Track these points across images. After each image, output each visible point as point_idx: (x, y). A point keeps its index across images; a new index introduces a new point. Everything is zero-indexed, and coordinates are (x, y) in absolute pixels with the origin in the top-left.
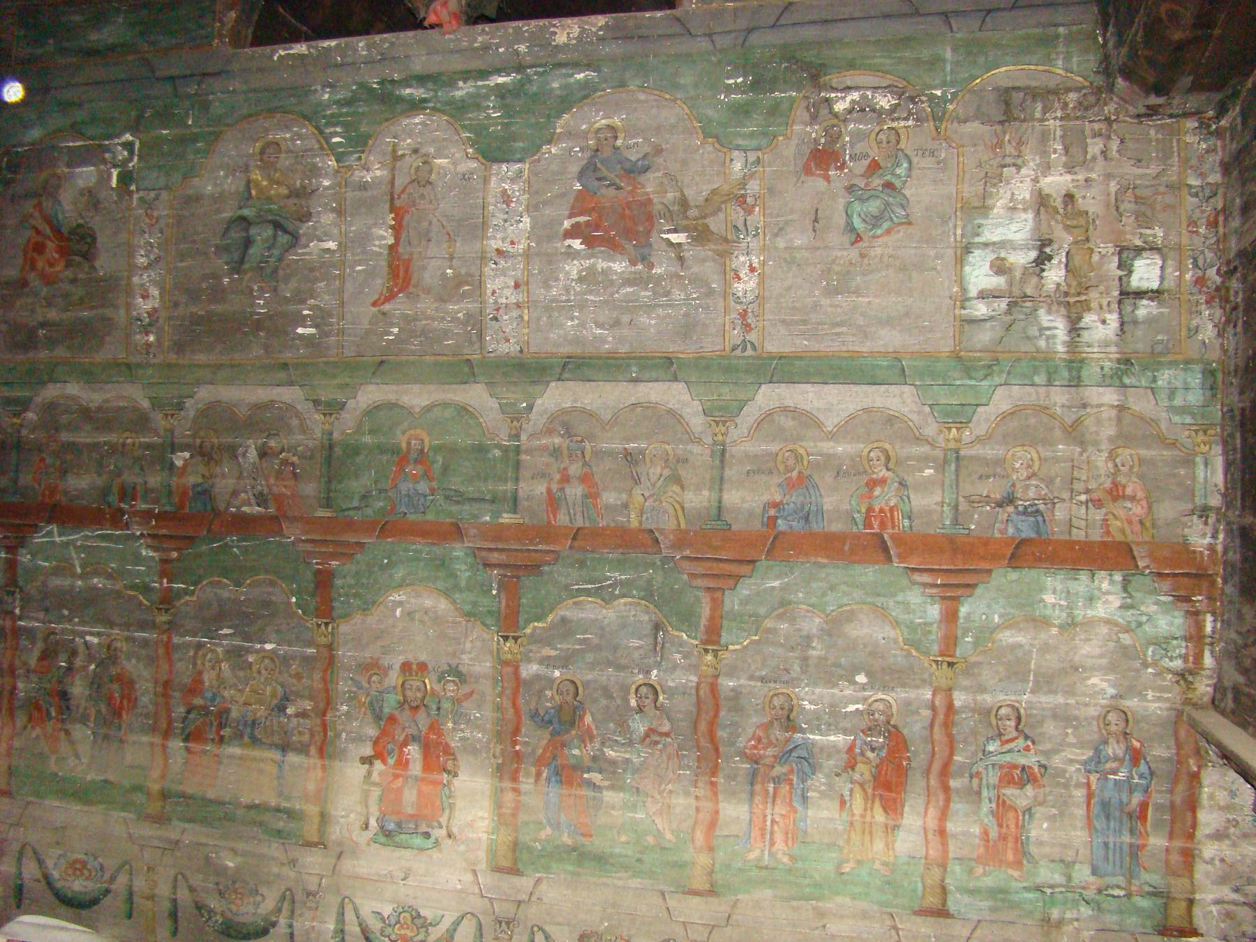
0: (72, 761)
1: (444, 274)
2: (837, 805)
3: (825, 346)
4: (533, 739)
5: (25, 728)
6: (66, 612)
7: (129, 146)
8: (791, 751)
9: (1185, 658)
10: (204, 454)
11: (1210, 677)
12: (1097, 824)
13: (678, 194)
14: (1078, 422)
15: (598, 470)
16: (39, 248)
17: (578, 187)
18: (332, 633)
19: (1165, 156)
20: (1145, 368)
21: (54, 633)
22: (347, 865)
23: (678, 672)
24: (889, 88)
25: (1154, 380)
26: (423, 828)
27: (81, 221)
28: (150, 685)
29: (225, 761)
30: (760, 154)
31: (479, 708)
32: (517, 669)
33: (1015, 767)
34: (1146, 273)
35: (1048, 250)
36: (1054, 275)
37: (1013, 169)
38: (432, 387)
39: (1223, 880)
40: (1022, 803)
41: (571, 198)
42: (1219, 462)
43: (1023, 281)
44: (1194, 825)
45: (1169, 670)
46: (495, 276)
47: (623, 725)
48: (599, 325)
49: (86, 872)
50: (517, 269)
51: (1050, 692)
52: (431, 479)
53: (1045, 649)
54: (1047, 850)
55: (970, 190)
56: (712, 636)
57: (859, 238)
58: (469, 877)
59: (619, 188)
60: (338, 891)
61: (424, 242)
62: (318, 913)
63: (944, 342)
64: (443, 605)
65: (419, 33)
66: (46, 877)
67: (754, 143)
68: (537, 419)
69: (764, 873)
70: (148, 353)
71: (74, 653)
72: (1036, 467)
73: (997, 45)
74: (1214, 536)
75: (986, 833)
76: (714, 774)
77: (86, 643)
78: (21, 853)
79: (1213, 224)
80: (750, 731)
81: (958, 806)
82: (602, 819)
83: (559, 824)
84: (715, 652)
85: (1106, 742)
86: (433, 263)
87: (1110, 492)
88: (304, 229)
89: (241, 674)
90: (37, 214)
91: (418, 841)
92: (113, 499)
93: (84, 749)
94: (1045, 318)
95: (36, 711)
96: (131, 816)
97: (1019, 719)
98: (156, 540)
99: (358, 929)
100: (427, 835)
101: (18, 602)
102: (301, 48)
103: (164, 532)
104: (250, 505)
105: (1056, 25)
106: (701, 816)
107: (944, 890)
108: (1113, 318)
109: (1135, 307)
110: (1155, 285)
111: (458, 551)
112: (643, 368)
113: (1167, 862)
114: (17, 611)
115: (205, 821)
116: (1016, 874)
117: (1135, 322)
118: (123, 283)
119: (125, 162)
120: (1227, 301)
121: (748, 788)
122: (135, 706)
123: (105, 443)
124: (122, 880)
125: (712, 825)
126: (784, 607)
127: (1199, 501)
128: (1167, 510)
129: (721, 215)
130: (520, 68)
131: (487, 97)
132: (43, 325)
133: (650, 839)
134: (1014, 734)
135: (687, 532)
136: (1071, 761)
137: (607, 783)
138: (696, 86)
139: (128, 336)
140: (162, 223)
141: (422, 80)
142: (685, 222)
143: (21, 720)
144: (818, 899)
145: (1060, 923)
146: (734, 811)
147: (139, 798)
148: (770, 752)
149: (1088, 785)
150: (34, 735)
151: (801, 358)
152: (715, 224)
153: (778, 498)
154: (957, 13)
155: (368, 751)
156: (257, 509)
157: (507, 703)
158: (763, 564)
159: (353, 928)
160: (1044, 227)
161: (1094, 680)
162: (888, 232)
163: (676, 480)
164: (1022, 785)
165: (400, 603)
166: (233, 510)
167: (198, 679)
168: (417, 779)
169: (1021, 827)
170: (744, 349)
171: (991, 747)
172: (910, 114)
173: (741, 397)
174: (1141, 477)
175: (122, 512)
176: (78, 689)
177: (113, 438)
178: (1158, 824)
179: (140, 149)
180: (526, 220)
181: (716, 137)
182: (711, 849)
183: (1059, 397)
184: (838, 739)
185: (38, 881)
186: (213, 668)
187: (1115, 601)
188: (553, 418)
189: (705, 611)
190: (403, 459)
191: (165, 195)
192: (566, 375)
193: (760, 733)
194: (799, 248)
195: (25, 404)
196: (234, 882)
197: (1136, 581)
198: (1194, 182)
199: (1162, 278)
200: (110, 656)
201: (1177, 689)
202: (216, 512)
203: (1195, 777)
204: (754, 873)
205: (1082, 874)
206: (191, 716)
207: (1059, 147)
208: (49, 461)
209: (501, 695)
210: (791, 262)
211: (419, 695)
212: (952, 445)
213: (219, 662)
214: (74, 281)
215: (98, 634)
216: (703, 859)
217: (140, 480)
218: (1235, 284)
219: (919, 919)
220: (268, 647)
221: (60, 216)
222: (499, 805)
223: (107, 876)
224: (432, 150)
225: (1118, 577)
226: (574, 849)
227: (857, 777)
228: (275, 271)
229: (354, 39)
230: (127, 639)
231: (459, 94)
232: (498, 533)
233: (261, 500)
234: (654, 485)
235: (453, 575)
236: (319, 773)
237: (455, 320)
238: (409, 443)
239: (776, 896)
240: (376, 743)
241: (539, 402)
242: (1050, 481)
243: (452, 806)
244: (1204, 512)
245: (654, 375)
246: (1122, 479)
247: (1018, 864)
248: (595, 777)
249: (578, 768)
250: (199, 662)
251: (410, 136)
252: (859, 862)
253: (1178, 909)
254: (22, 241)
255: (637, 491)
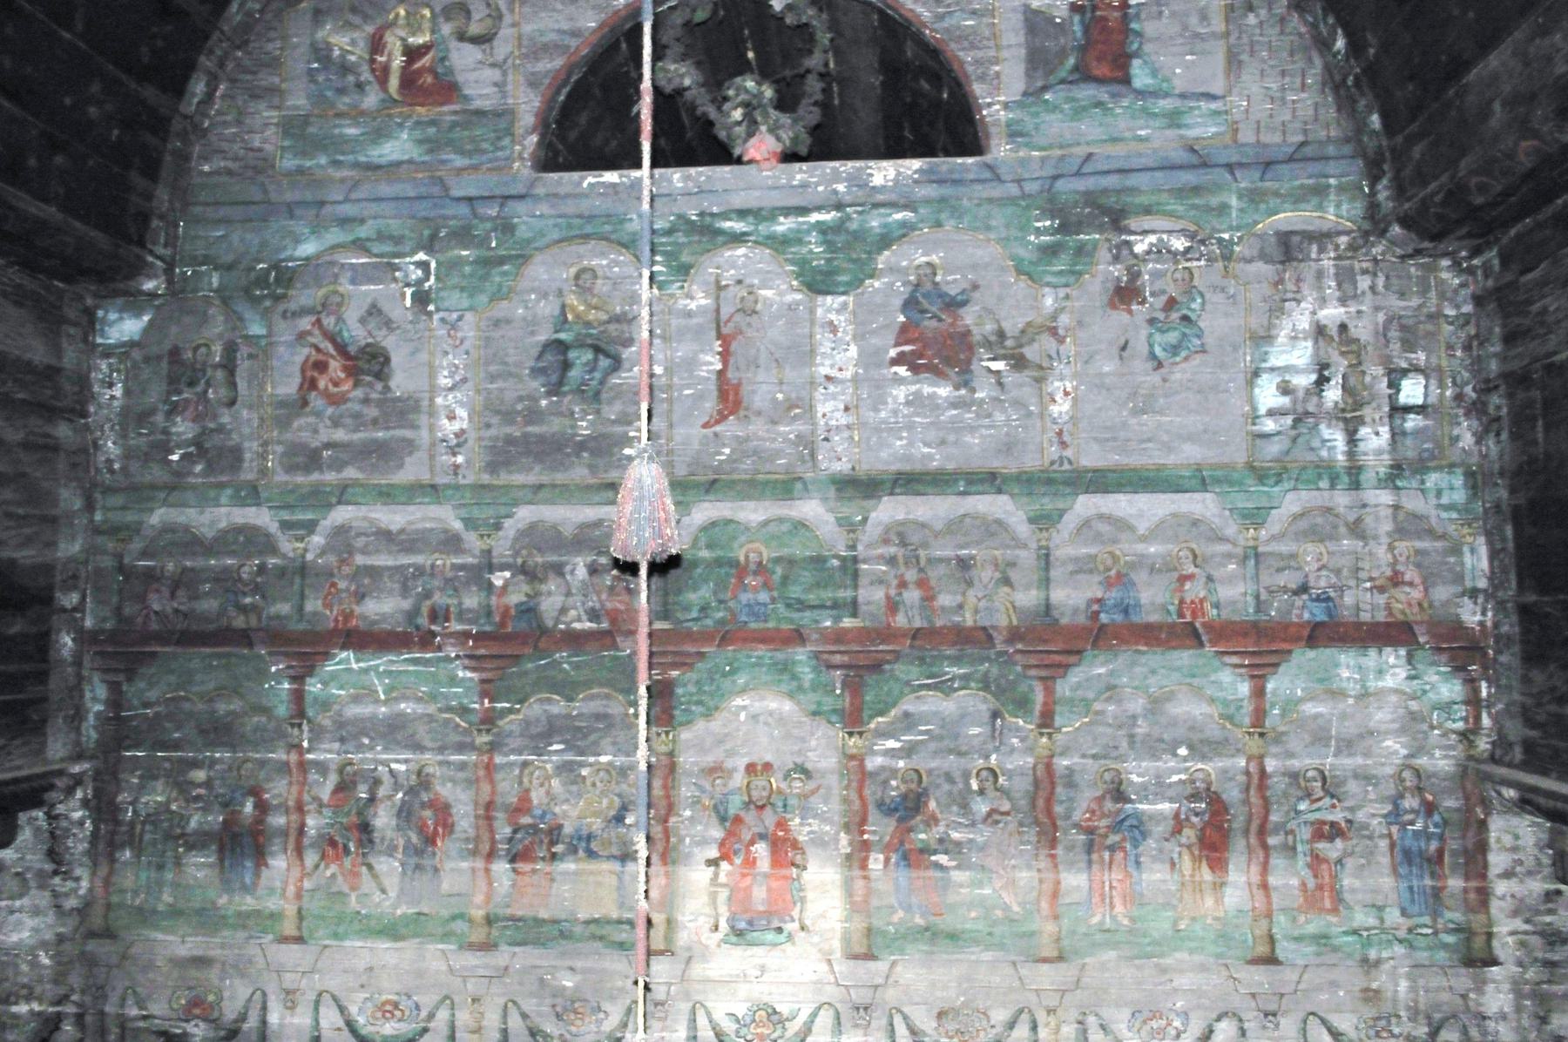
0: (377, 897)
1: (774, 400)
2: (1168, 866)
3: (1135, 460)
4: (880, 828)
5: (317, 867)
6: (366, 741)
7: (424, 266)
8: (1123, 820)
9: (1465, 719)
10: (527, 572)
11: (1488, 736)
12: (1401, 870)
13: (995, 326)
14: (1359, 520)
15: (934, 574)
16: (321, 366)
17: (902, 318)
18: (674, 741)
19: (1424, 291)
20: (1415, 472)
21: (351, 764)
22: (697, 970)
23: (1015, 755)
24: (1183, 232)
25: (1423, 482)
26: (776, 924)
27: (370, 340)
28: (470, 808)
29: (558, 878)
30: (1068, 290)
31: (826, 802)
32: (862, 761)
33: (1324, 823)
34: (1412, 391)
35: (1326, 373)
36: (1333, 394)
37: (1294, 304)
38: (767, 503)
39: (1515, 913)
40: (1334, 855)
41: (897, 328)
42: (1483, 551)
43: (1305, 401)
44: (1486, 866)
45: (1454, 732)
46: (826, 400)
47: (965, 807)
48: (927, 444)
49: (398, 1013)
50: (848, 395)
51: (1350, 755)
52: (771, 589)
53: (1343, 716)
54: (1360, 896)
55: (1256, 322)
56: (1046, 721)
57: (1160, 365)
58: (824, 967)
59: (940, 320)
60: (687, 995)
61: (753, 368)
62: (668, 1022)
63: (1237, 454)
64: (787, 706)
65: (736, 168)
66: (351, 1025)
67: (1063, 280)
68: (872, 531)
69: (1107, 935)
70: (456, 474)
71: (377, 782)
72: (1325, 560)
73: (1276, 194)
74: (1484, 613)
75: (1304, 884)
76: (1053, 847)
77: (391, 771)
78: (317, 1003)
79: (1467, 348)
80: (1084, 805)
81: (1277, 861)
82: (952, 898)
83: (910, 906)
84: (1050, 735)
85: (1402, 796)
86: (764, 387)
87: (1391, 579)
88: (626, 353)
89: (574, 788)
90: (317, 332)
91: (770, 936)
92: (423, 621)
93: (392, 883)
94: (1326, 432)
95: (331, 846)
96: (452, 947)
97: (1324, 779)
98: (475, 661)
99: (711, 1034)
100: (779, 930)
101: (305, 735)
102: (611, 177)
103: (482, 651)
104: (579, 620)
105: (1327, 177)
106: (1044, 886)
107: (1272, 940)
108: (1385, 431)
109: (1404, 420)
110: (1420, 401)
111: (801, 654)
112: (970, 482)
113: (1466, 900)
114: (305, 744)
115: (538, 942)
116: (1334, 919)
117: (1404, 433)
118: (425, 403)
119: (420, 282)
120: (1485, 413)
121: (1085, 857)
122: (452, 832)
123: (409, 565)
124: (443, 1015)
125: (1055, 895)
126: (1110, 690)
127: (1469, 584)
128: (1441, 593)
129: (1036, 345)
130: (839, 206)
131: (808, 232)
132: (328, 446)
133: (999, 913)
134: (1321, 794)
135: (1017, 627)
136: (1374, 815)
137: (954, 863)
138: (1007, 226)
139: (432, 457)
140: (467, 344)
141: (742, 214)
142: (1003, 352)
143: (311, 858)
144: (1162, 955)
145: (1378, 963)
146: (1075, 880)
147: (460, 926)
148: (1104, 823)
149: (1390, 835)
150: (328, 873)
151: (1114, 471)
152: (1030, 352)
153: (1099, 595)
154: (1241, 165)
155: (714, 853)
156: (588, 625)
157: (854, 796)
158: (1089, 654)
159: (705, 1033)
160: (1322, 353)
161: (1389, 743)
162: (1186, 359)
163: (1007, 581)
164: (1331, 839)
165: (744, 708)
166: (562, 626)
167: (525, 798)
168: (766, 876)
169: (1335, 877)
170: (1061, 464)
171: (1302, 806)
172: (1202, 255)
173: (1061, 506)
174: (1418, 566)
175: (434, 634)
176: (383, 820)
177: (419, 559)
178: (1454, 869)
179: (437, 269)
180: (853, 351)
181: (1027, 274)
182: (1056, 917)
183: (1341, 500)
184: (1166, 807)
185: (339, 1029)
186: (542, 785)
187: (1402, 673)
188: (887, 530)
189: (1039, 697)
190: (741, 570)
191: (469, 316)
192: (898, 490)
193: (1094, 806)
194: (1108, 374)
195: (311, 527)
196: (573, 1002)
197: (1419, 654)
198: (1450, 312)
199: (1426, 395)
200: (423, 781)
201: (1461, 747)
202: (543, 631)
203: (1483, 825)
204: (1098, 937)
205: (1393, 916)
206: (519, 836)
207: (1333, 284)
208: (342, 585)
209: (847, 788)
210: (1101, 386)
211: (765, 794)
212: (1251, 543)
213: (548, 778)
214: (366, 401)
215: (406, 761)
216: (1050, 927)
217: (453, 601)
218: (1495, 400)
219: (1253, 968)
220: (604, 759)
221: (346, 334)
222: (849, 892)
223: (424, 1014)
224: (756, 281)
225: (1403, 652)
226: (927, 929)
227: (1184, 840)
228: (597, 394)
229: (670, 170)
230: (441, 763)
231: (780, 229)
232: (839, 636)
233: (594, 615)
234: (985, 587)
235: (794, 677)
236: (663, 881)
237: (786, 440)
238: (747, 557)
239: (1119, 957)
240: (722, 844)
241: (873, 515)
242: (1338, 572)
243: (803, 900)
244: (1473, 593)
245: (980, 488)
246: (1400, 568)
247: (1335, 911)
248: (942, 859)
249: (926, 851)
250: (525, 780)
251: (733, 267)
252: (1194, 919)
253: (1479, 942)
254: (299, 359)
255: (971, 593)
